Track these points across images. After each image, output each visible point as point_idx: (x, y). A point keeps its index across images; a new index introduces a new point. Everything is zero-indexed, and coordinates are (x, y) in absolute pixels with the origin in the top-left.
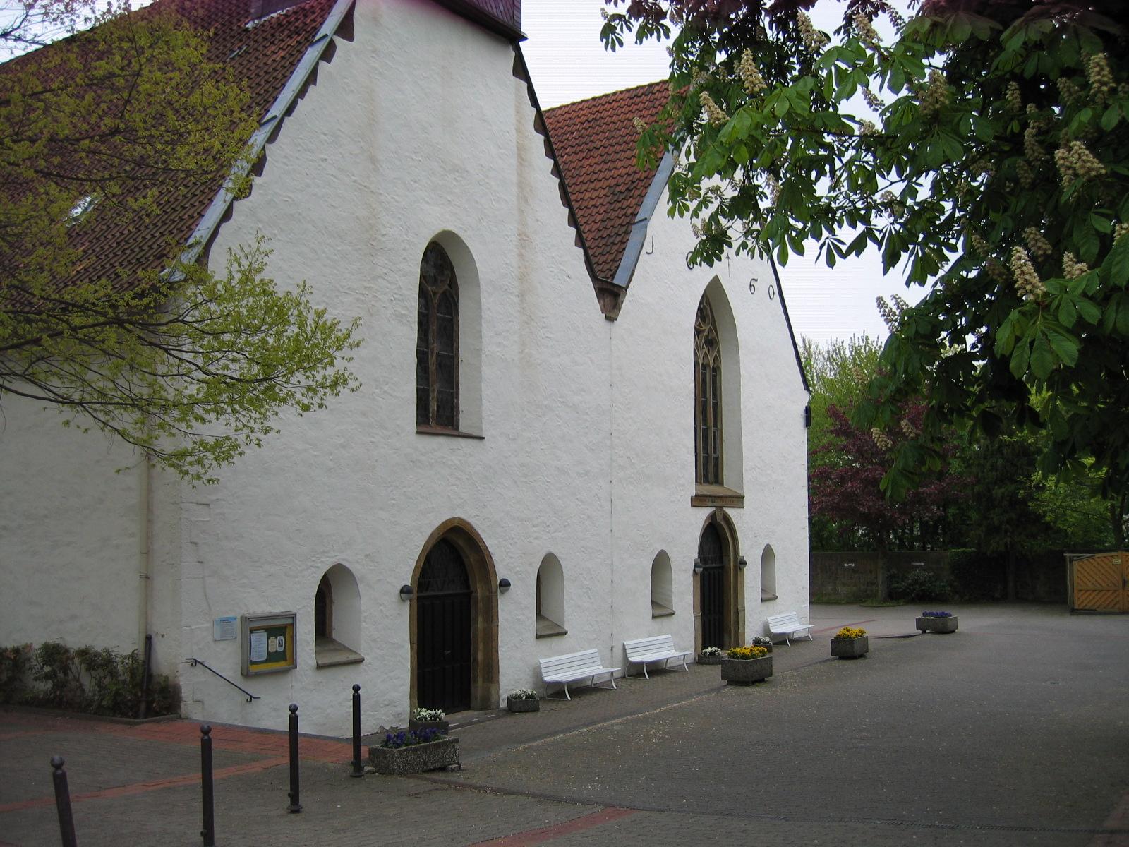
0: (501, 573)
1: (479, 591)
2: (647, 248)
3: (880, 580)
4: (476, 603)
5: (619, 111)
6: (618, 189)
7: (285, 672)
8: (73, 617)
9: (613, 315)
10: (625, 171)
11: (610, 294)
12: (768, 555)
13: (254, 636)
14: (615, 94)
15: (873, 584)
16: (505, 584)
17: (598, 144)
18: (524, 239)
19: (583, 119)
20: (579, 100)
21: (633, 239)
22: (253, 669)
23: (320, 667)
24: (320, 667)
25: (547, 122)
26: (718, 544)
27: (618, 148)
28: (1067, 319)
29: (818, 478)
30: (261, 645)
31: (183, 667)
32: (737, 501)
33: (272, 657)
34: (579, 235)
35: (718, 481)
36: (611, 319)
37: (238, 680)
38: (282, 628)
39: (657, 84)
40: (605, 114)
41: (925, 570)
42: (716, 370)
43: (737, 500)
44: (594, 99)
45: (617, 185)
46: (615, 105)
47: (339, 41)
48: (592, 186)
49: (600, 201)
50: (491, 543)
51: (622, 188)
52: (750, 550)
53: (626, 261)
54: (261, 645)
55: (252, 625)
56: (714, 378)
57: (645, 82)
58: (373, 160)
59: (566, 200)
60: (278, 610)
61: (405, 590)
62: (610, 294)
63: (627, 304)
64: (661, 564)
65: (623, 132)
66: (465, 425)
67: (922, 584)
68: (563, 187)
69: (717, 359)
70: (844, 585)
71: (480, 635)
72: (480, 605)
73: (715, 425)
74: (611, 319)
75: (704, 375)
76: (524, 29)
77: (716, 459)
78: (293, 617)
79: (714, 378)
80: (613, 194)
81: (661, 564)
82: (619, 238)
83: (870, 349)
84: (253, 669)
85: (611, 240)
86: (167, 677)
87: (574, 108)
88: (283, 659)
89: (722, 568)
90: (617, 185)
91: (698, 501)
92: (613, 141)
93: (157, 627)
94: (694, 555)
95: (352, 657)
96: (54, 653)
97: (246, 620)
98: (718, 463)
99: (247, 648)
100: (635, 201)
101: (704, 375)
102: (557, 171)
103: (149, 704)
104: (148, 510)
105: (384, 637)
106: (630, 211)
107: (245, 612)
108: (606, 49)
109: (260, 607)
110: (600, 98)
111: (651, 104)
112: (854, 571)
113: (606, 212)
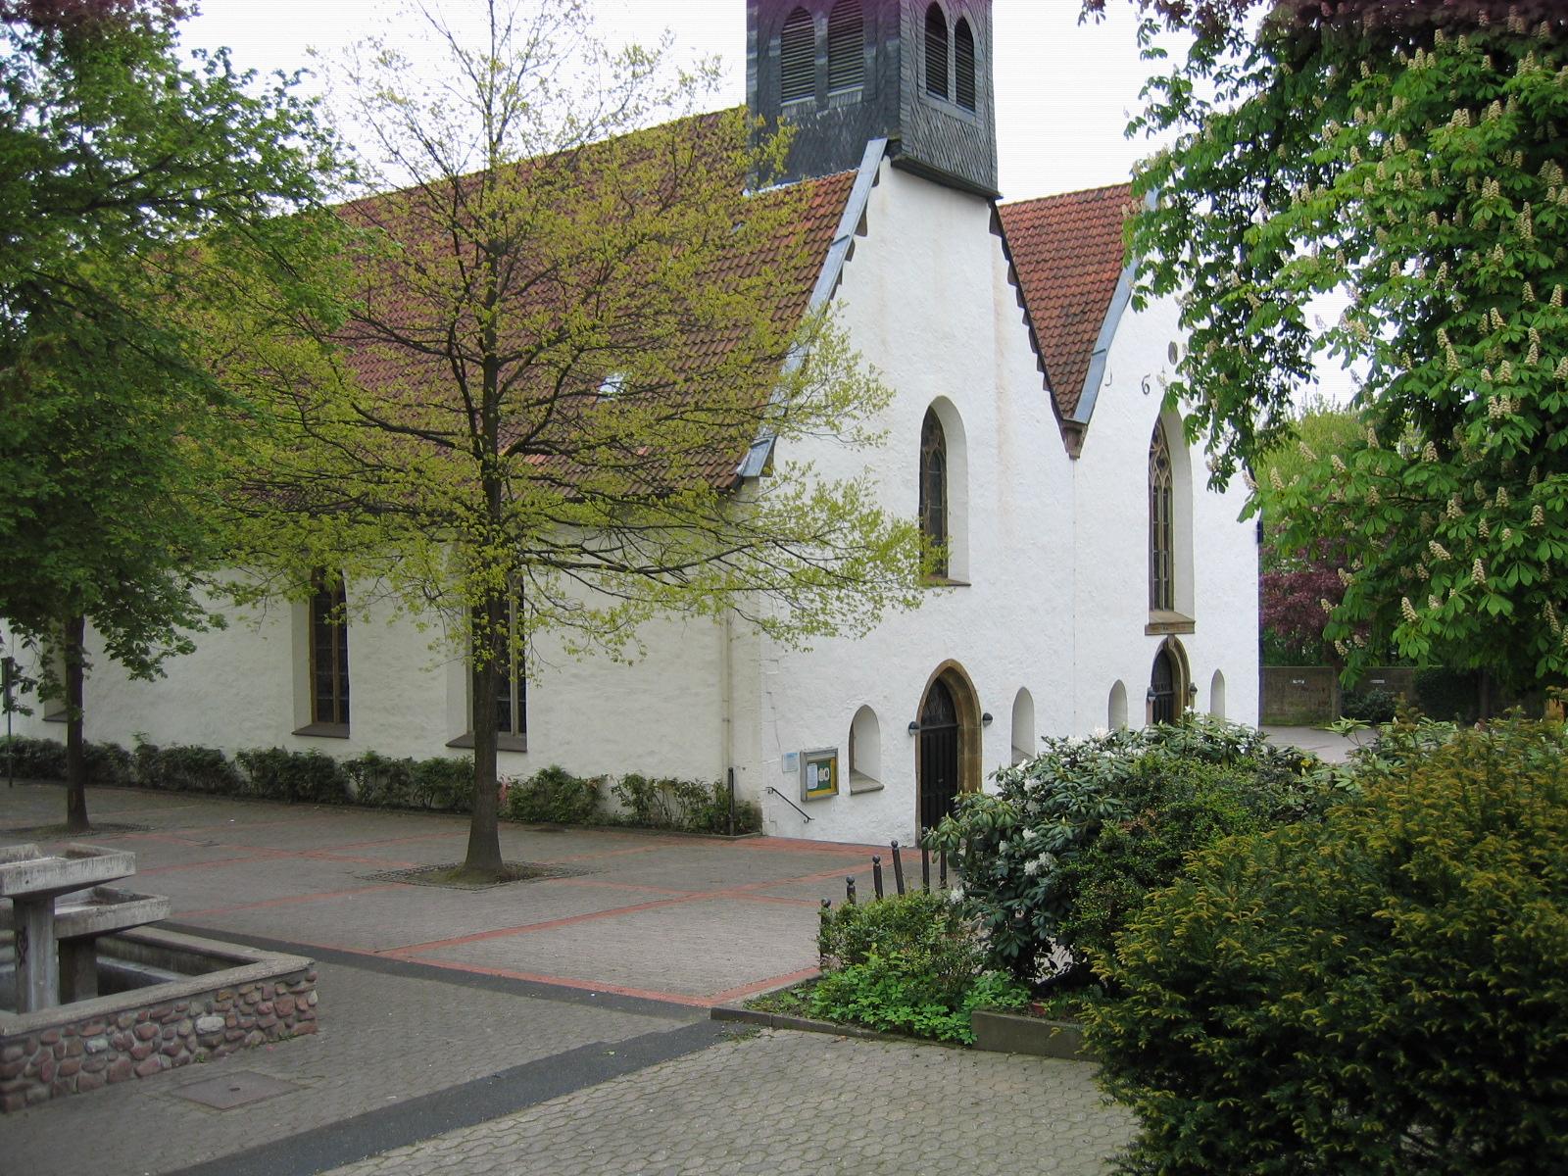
0: (985, 707)
1: (966, 725)
2: (1106, 380)
3: (1334, 700)
4: (962, 735)
5: (1067, 217)
6: (1073, 310)
7: (828, 798)
8: (652, 753)
9: (1074, 453)
10: (1079, 290)
11: (1073, 433)
12: (1218, 679)
13: (809, 769)
14: (1061, 196)
15: (1326, 703)
16: (988, 718)
17: (1047, 256)
18: (1000, 391)
19: (1028, 224)
20: (1022, 200)
21: (1093, 371)
22: (811, 795)
23: (852, 794)
24: (852, 794)
26: (1169, 668)
28: (1426, 631)
29: (1270, 587)
30: (815, 775)
31: (763, 794)
33: (822, 785)
35: (1169, 606)
36: (1074, 457)
37: (798, 804)
39: (1108, 189)
41: (1385, 689)
42: (1168, 491)
43: (1188, 626)
44: (1039, 200)
45: (1070, 305)
46: (1062, 210)
47: (858, 239)
48: (1043, 304)
49: (1053, 323)
50: (976, 680)
52: (1199, 675)
54: (815, 775)
56: (1166, 498)
57: (1095, 186)
58: (884, 342)
59: (1036, 346)
60: (824, 746)
62: (1073, 433)
63: (1089, 440)
64: (1117, 693)
66: (953, 573)
67: (1382, 705)
68: (1032, 333)
70: (1292, 704)
71: (966, 764)
72: (966, 737)
73: (1166, 548)
74: (1074, 457)
75: (1156, 497)
76: (1000, 189)
77: (1167, 583)
78: (835, 751)
79: (1166, 498)
80: (1067, 315)
81: (1117, 693)
82: (1076, 368)
83: (1325, 410)
84: (811, 795)
85: (1068, 369)
86: (748, 803)
87: (1017, 209)
88: (830, 785)
89: (1172, 695)
90: (1070, 305)
91: (1152, 629)
93: (738, 762)
94: (1148, 683)
95: (876, 785)
96: (635, 783)
99: (804, 777)
101: (1156, 497)
102: (1028, 319)
103: (736, 824)
104: (727, 666)
107: (802, 748)
108: (1241, 519)
109: (813, 744)
110: (1045, 199)
111: (1102, 213)
112: (1303, 688)
113: (1060, 336)
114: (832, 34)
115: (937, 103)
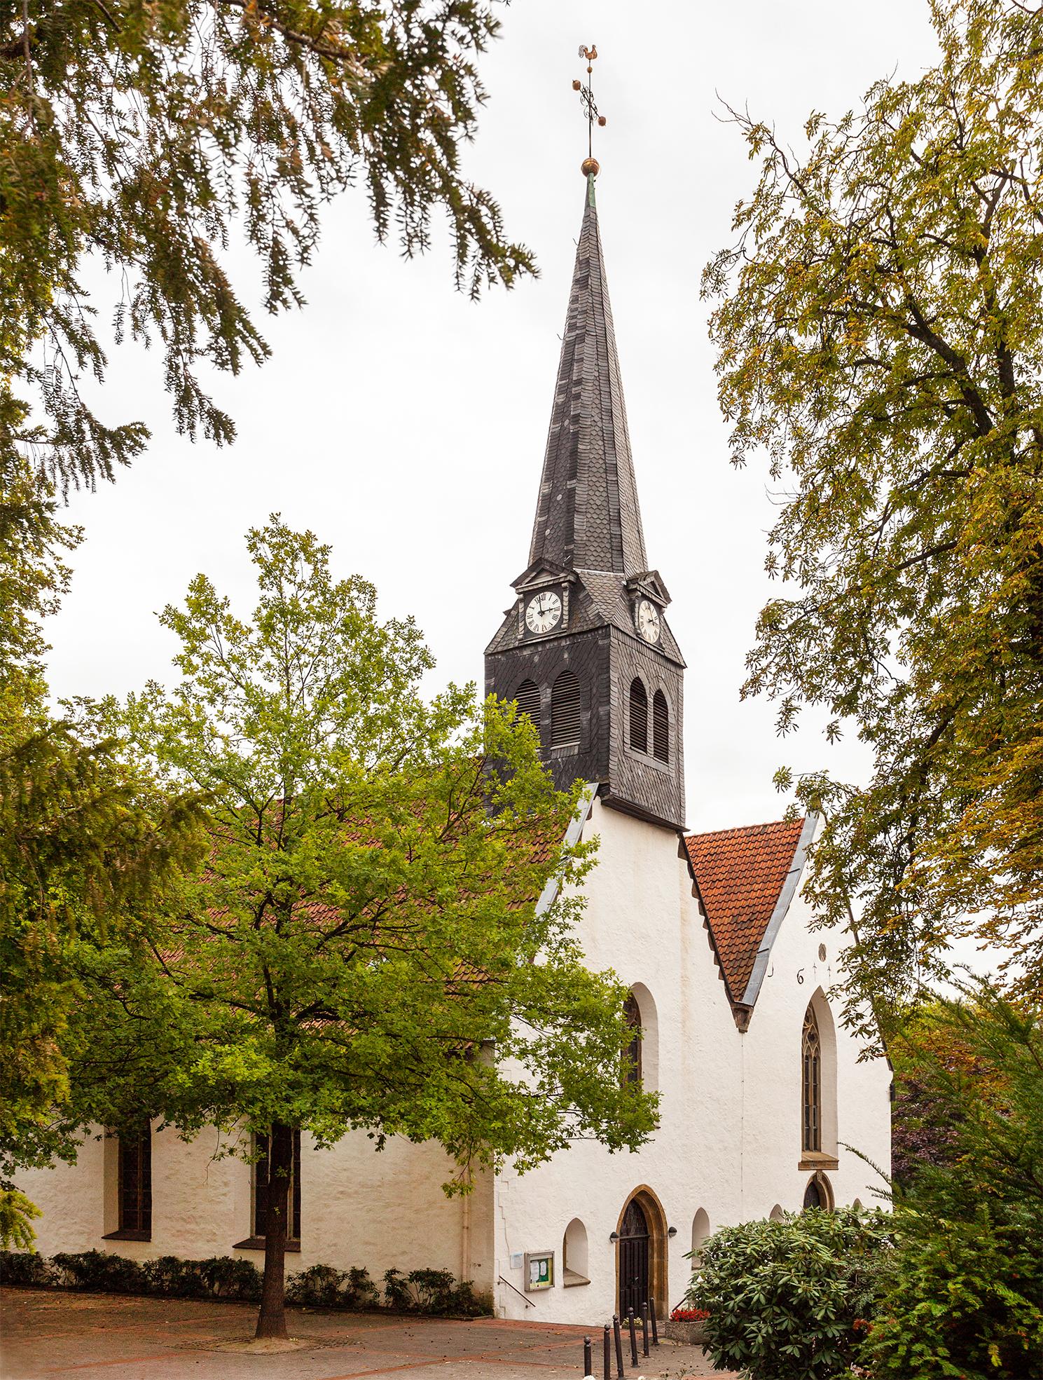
2: (769, 972)
11: (742, 1013)
16: (673, 1231)
23: (566, 1287)
24: (566, 1287)
25: (689, 848)
27: (739, 882)
32: (833, 1164)
34: (722, 971)
35: (817, 1148)
36: (742, 1031)
38: (548, 1259)
40: (725, 849)
42: (817, 1059)
51: (745, 918)
53: (752, 984)
55: (529, 1259)
59: (713, 946)
60: (543, 1249)
61: (613, 1236)
62: (742, 1013)
65: (744, 867)
68: (711, 935)
69: (818, 1050)
74: (742, 1031)
82: (743, 963)
91: (804, 1165)
92: (734, 875)
97: (527, 1255)
98: (817, 1132)
99: (527, 1273)
100: (756, 931)
102: (707, 924)
105: (602, 1262)
106: (753, 939)
109: (534, 1248)
114: (555, 701)
115: (638, 756)
